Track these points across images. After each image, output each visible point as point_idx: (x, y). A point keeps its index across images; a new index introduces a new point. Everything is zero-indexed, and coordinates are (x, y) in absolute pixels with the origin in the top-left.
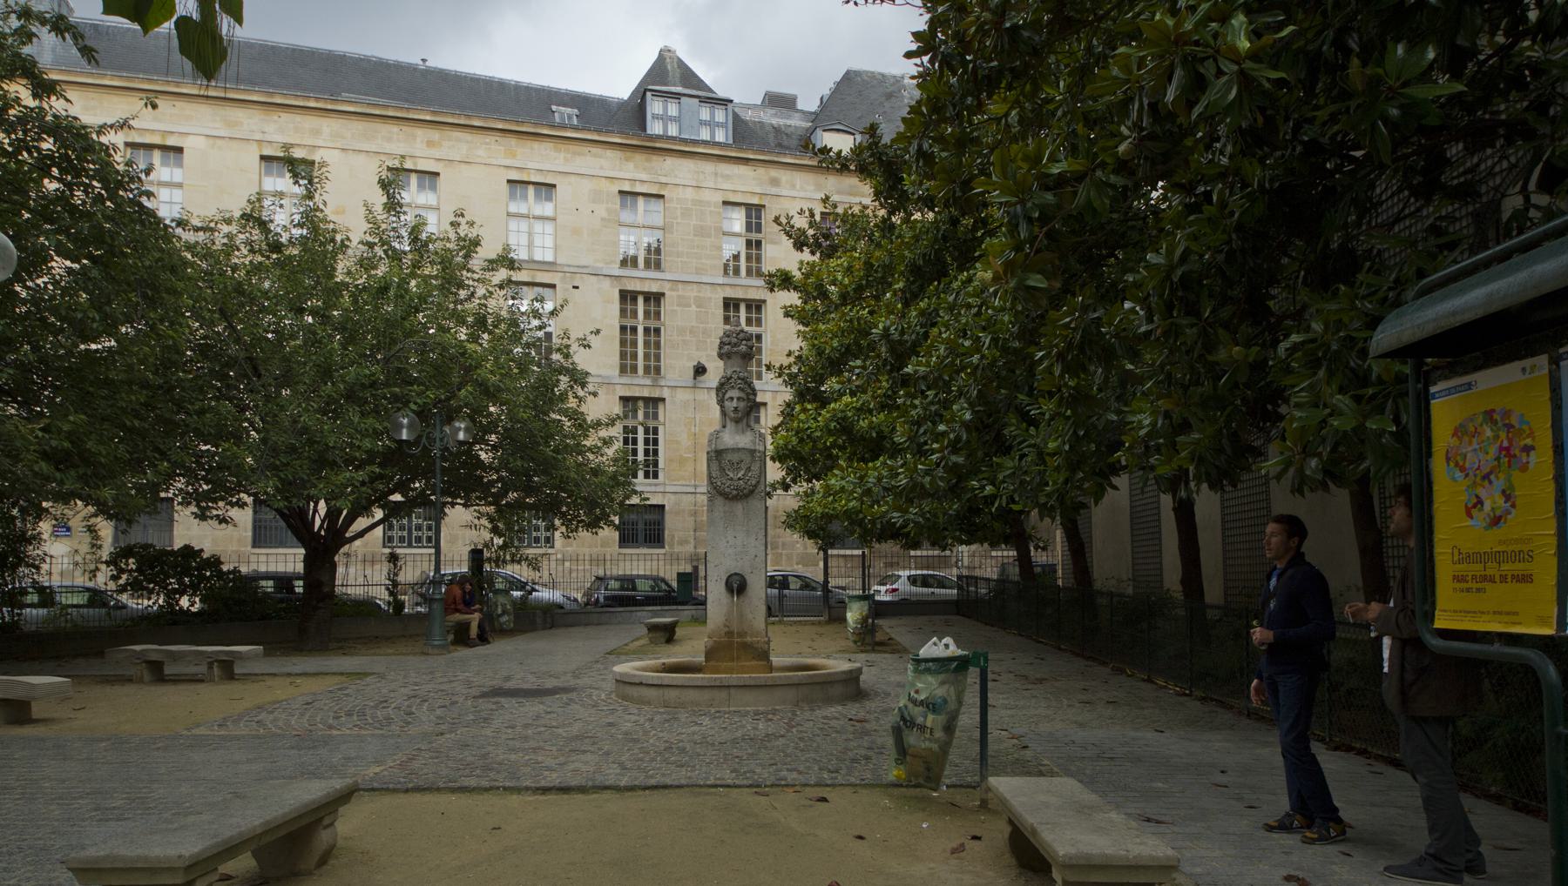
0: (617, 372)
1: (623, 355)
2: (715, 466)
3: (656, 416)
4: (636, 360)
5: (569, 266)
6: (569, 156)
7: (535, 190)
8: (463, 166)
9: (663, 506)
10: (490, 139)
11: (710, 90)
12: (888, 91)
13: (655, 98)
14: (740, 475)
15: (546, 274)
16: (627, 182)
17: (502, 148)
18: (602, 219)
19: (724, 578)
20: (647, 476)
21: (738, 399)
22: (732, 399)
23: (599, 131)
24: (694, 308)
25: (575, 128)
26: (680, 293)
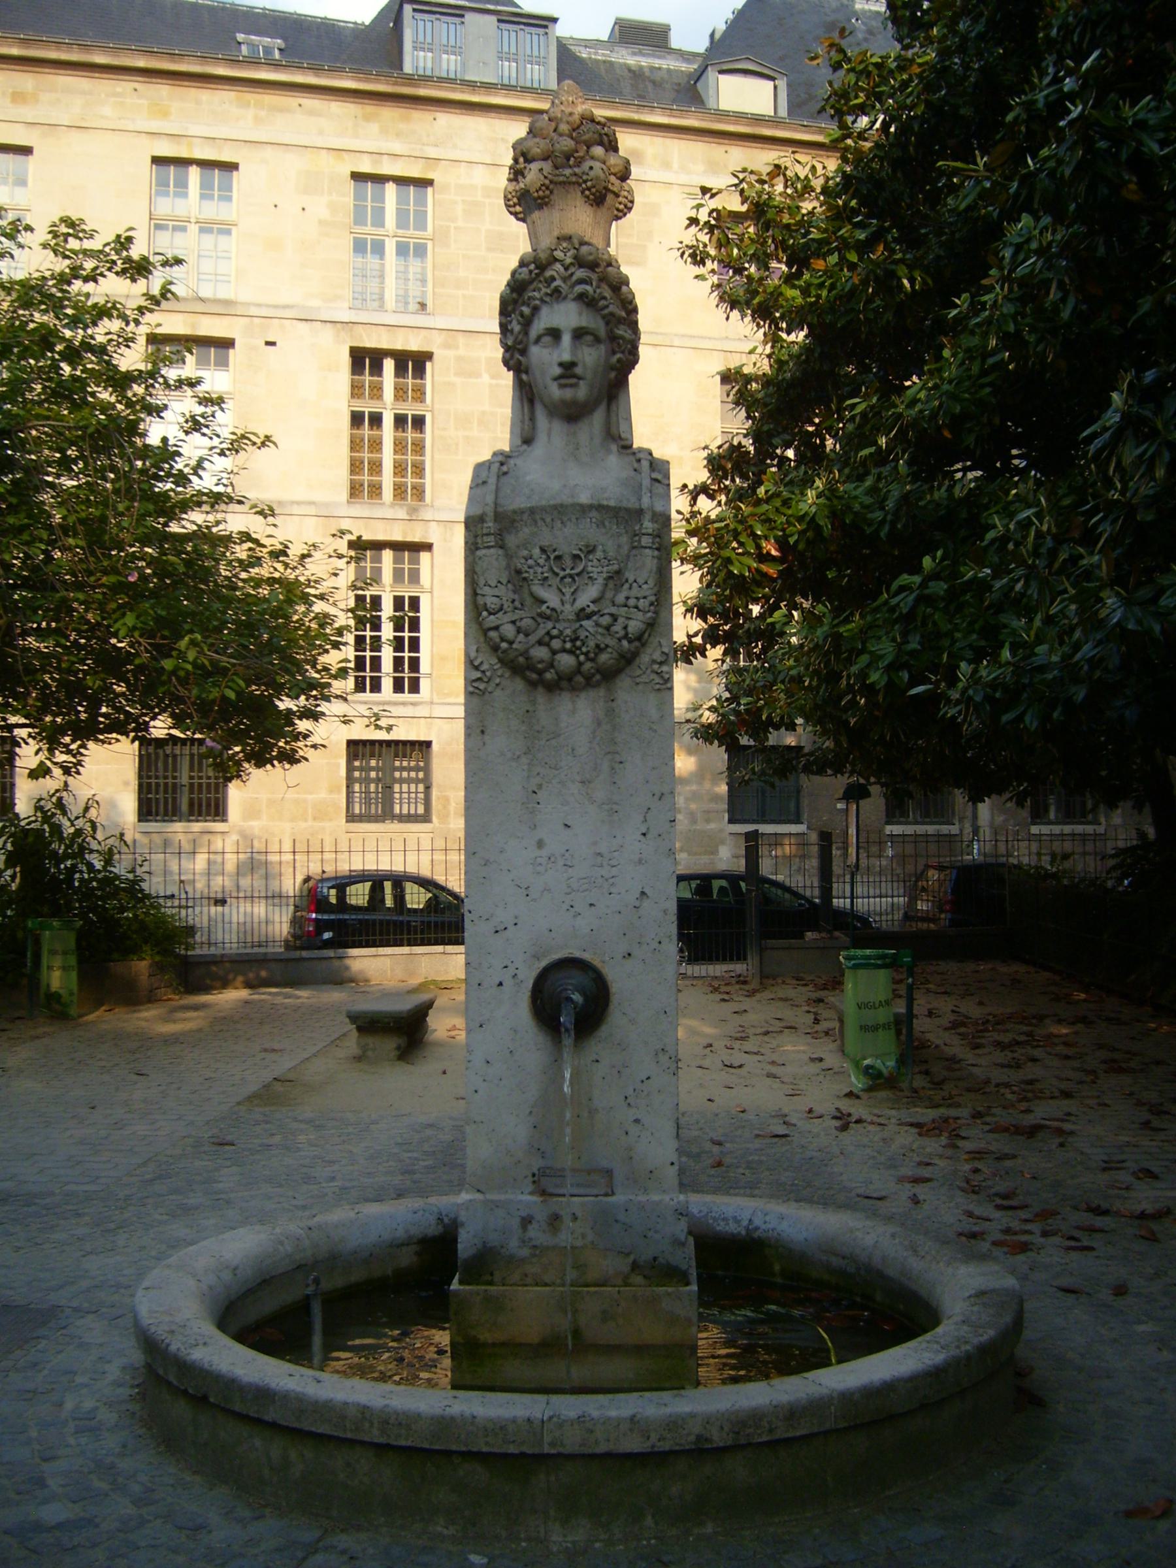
0: (344, 495)
1: (355, 466)
2: (491, 557)
3: (415, 577)
4: (380, 450)
5: (259, 305)
6: (263, 113)
7: (202, 176)
8: (75, 135)
9: (428, 744)
10: (124, 87)
11: (517, 6)
12: (829, 19)
13: (418, 16)
14: (584, 600)
15: (217, 319)
16: (365, 157)
17: (144, 102)
18: (320, 222)
19: (529, 977)
20: (398, 687)
21: (579, 334)
22: (555, 334)
23: (316, 69)
24: (486, 378)
25: (276, 65)
26: (461, 352)
